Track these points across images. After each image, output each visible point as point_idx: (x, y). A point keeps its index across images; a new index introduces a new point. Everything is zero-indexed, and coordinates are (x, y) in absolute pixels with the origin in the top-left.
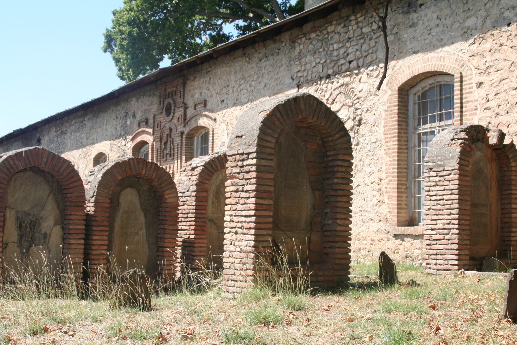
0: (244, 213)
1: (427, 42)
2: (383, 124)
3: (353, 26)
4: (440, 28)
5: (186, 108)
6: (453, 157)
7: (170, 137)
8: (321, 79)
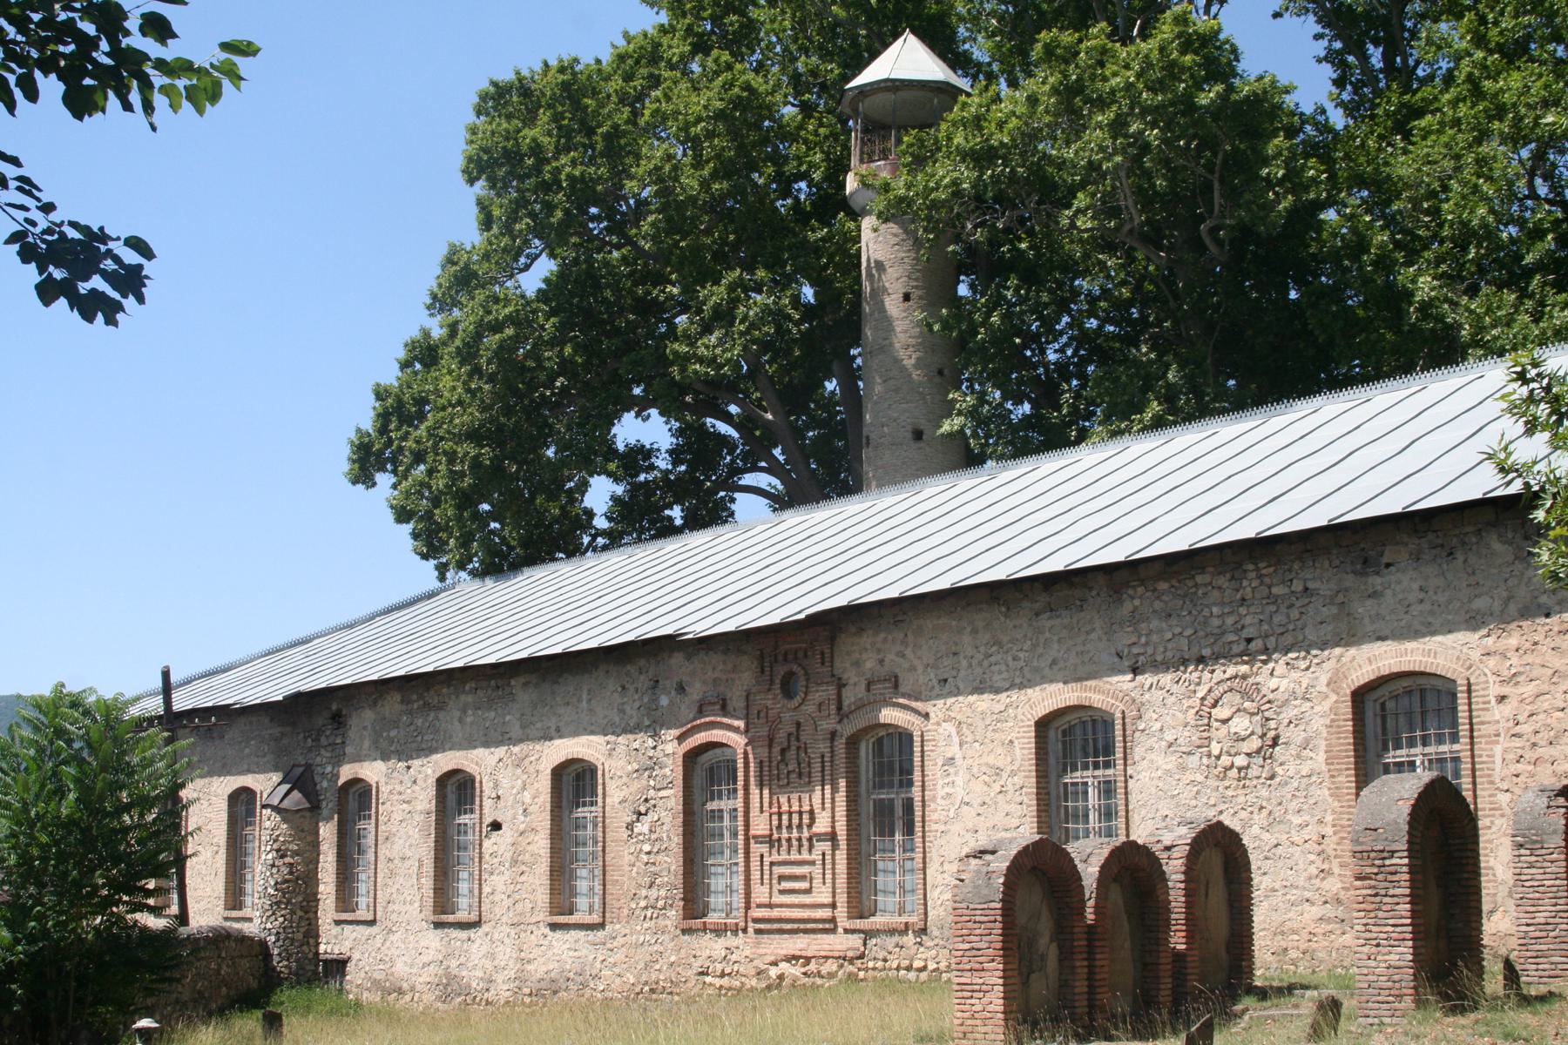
0: (1391, 922)
1: (1403, 623)
2: (1323, 748)
3: (1249, 585)
4: (1427, 606)
5: (841, 686)
6: (1555, 832)
7: (798, 739)
8: (1185, 662)
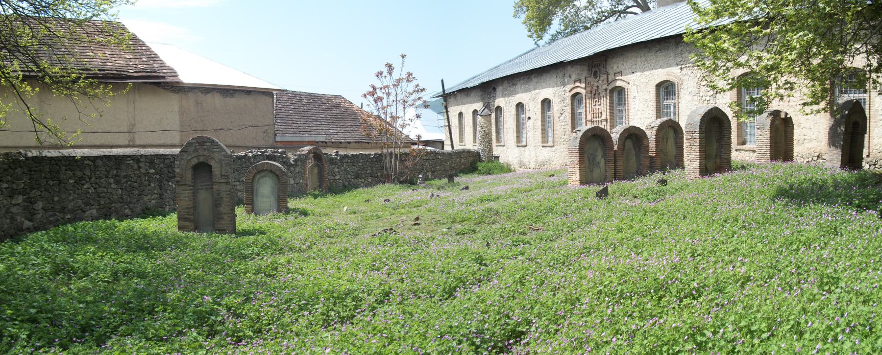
5: (608, 74)
